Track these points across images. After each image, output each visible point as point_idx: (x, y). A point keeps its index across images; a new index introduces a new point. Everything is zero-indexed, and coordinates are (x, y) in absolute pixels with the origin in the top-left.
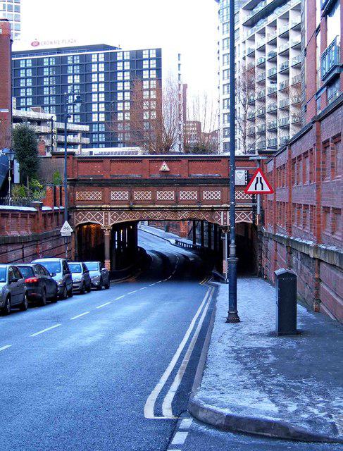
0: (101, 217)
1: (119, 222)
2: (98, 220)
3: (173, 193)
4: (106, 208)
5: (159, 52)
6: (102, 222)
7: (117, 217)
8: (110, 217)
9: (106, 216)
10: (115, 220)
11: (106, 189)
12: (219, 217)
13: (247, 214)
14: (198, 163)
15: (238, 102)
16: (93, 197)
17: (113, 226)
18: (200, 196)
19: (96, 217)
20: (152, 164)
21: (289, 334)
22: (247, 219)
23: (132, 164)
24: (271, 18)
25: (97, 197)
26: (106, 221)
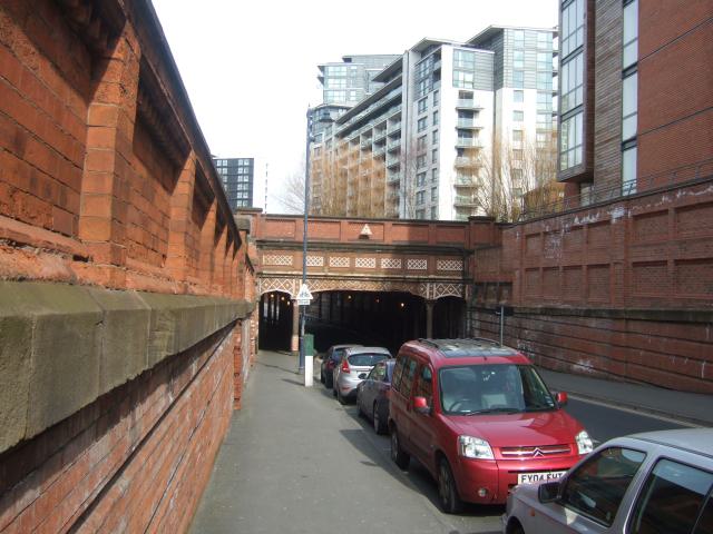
0: (290, 286)
3: (374, 260)
4: (298, 275)
5: (251, 160)
15: (178, 409)
18: (404, 265)
22: (455, 293)
24: (365, 129)
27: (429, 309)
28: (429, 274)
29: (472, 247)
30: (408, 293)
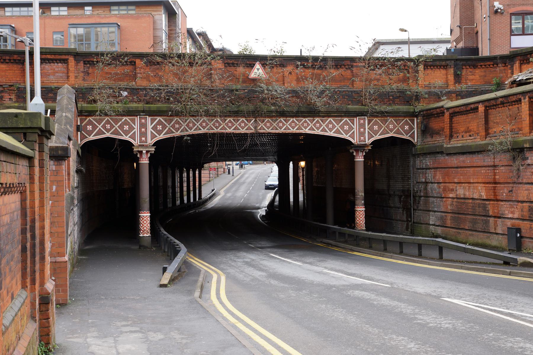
0: (131, 128)
6: (133, 137)
7: (380, 127)
8: (150, 127)
9: (362, 126)
26: (143, 134)
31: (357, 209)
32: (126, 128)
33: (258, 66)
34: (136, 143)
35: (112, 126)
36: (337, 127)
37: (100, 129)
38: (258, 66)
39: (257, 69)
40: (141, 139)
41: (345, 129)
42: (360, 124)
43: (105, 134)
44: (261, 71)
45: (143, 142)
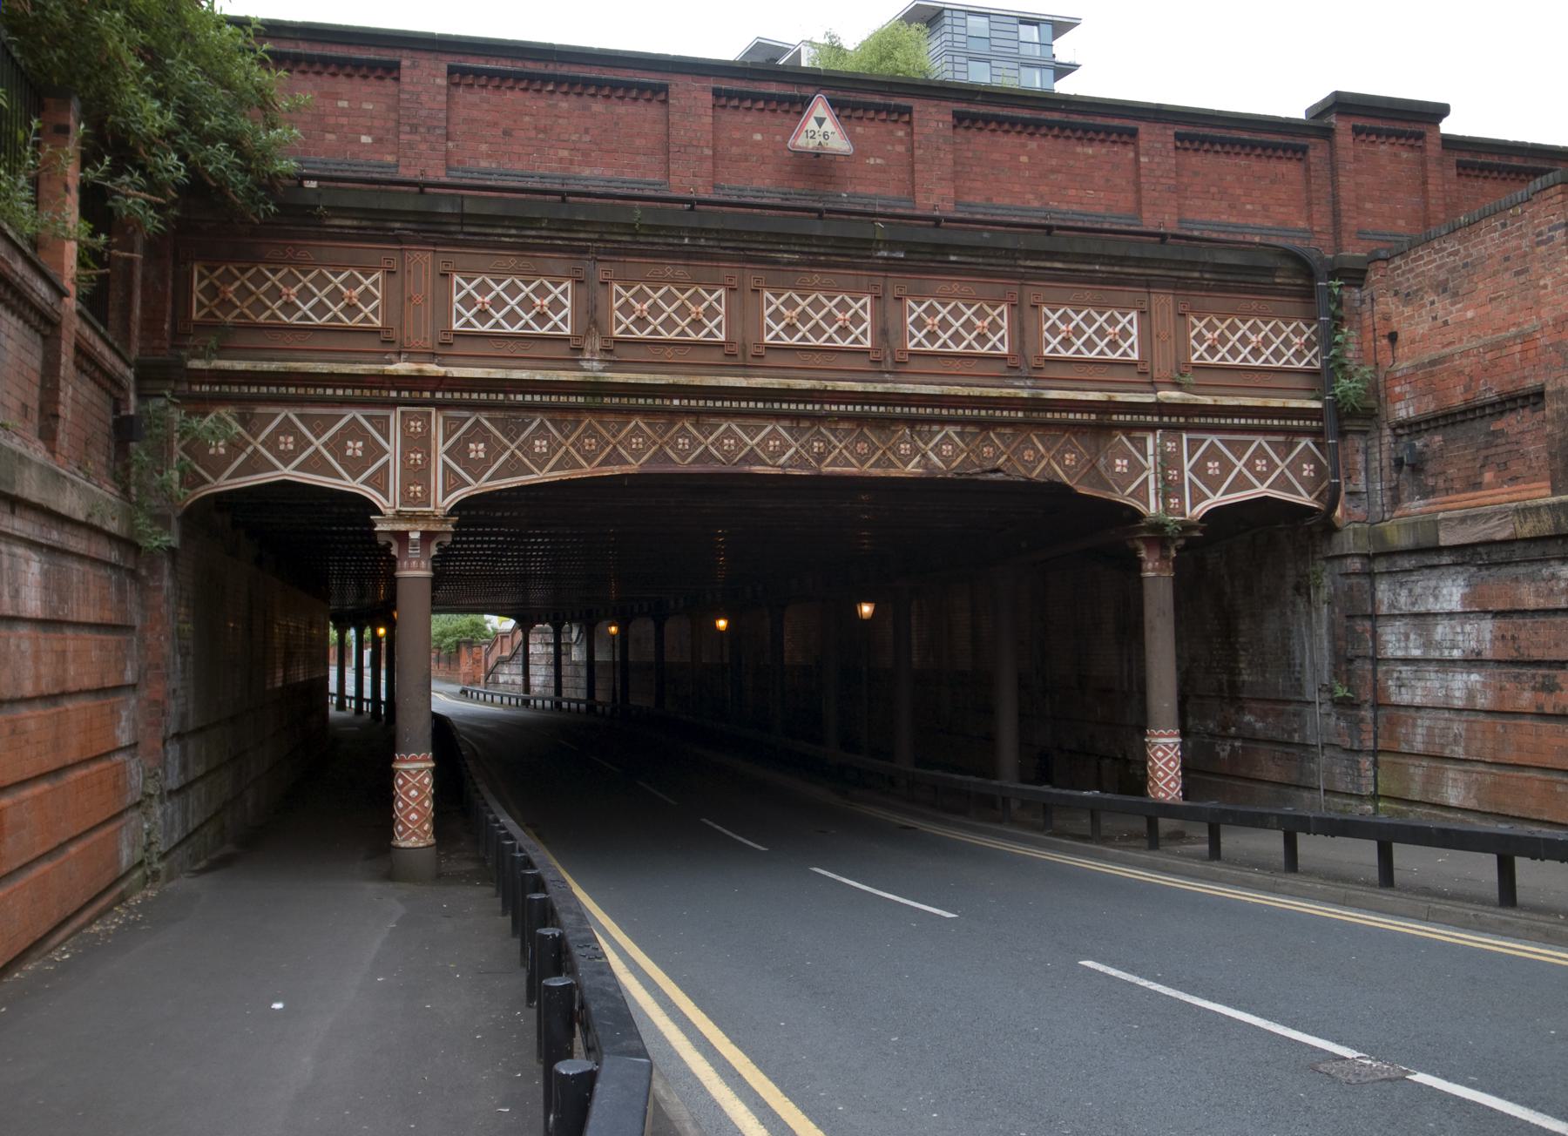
0: (373, 451)
1: (608, 471)
2: (355, 468)
6: (382, 486)
7: (493, 451)
8: (440, 449)
9: (418, 442)
10: (476, 468)
11: (422, 261)
12: (1136, 468)
13: (1285, 449)
14: (1009, 141)
16: (320, 309)
17: (459, 507)
19: (337, 446)
20: (727, 117)
21: (1519, 938)
22: (1282, 483)
23: (598, 107)
25: (697, 324)
26: (417, 474)
27: (1155, 570)
28: (1154, 386)
29: (1354, 251)
30: (1056, 492)
31: (1153, 741)
32: (355, 448)
33: (820, 108)
34: (391, 504)
35: (303, 444)
36: (1282, 466)
37: (317, 451)
38: (820, 108)
39: (816, 118)
40: (404, 492)
41: (349, 452)
42: (1164, 455)
43: (276, 469)
44: (829, 126)
45: (415, 501)
